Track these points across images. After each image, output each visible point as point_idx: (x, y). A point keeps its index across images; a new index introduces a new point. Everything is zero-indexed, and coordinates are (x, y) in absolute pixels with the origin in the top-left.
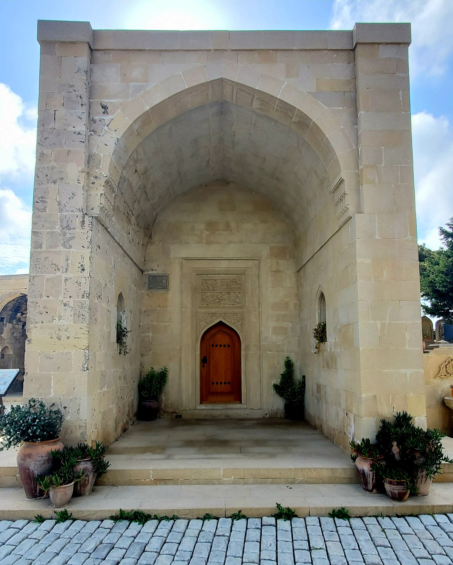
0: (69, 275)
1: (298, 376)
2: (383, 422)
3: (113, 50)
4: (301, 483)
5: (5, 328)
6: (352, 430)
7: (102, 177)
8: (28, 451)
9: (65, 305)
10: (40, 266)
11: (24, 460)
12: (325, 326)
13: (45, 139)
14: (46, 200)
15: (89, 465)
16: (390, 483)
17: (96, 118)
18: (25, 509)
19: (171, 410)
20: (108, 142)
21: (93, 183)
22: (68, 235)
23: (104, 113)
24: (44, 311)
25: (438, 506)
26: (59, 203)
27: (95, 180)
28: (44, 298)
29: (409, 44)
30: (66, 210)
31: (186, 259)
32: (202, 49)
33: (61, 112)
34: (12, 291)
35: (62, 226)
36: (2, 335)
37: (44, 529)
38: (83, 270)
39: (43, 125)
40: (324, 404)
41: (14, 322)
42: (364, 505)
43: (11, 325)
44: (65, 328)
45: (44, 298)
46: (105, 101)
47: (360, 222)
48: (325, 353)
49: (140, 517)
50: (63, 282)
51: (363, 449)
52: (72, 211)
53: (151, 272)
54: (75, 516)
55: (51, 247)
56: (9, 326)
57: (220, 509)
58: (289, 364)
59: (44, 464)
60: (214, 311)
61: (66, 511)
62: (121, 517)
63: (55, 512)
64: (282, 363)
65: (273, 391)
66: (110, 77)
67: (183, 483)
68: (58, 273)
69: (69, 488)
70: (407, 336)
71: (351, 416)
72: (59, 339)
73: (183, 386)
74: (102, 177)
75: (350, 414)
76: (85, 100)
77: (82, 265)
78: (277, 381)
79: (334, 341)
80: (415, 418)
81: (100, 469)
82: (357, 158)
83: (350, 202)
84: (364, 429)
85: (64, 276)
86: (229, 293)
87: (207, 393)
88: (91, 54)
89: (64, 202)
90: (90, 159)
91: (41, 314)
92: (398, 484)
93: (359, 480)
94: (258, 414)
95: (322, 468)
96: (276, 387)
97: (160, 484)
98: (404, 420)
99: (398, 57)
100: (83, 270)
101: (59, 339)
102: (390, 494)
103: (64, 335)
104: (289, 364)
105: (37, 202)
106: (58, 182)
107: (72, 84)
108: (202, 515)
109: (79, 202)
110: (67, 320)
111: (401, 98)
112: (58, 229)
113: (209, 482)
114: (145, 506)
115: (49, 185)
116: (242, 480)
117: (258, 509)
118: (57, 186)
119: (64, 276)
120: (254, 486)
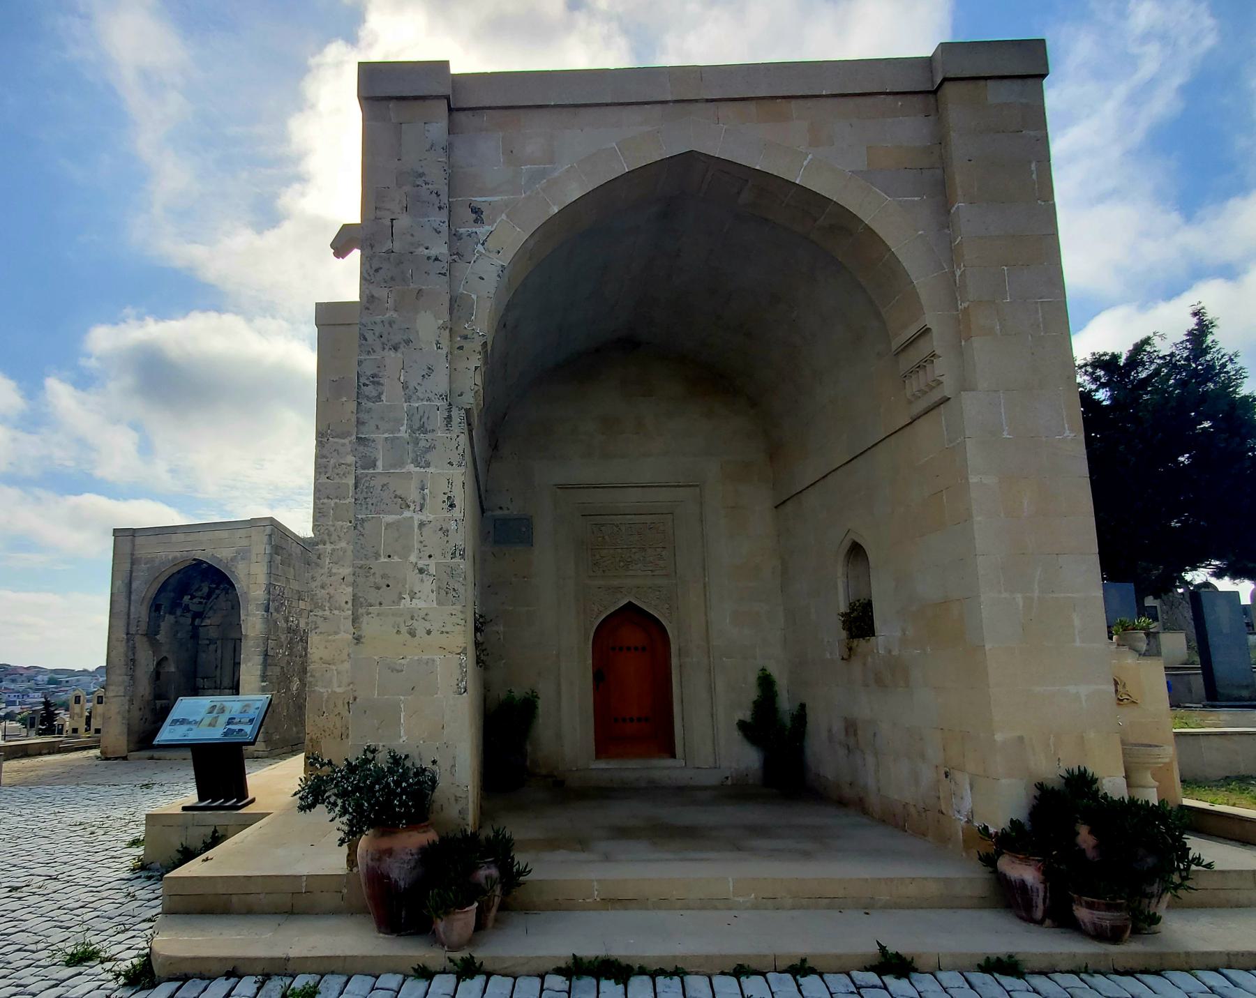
0: (425, 516)
1: (785, 704)
2: (1040, 786)
3: (489, 108)
4: (886, 907)
5: (162, 624)
6: (967, 804)
7: (476, 336)
8: (386, 843)
9: (421, 571)
10: (374, 501)
11: (379, 859)
12: (868, 606)
13: (377, 271)
14: (381, 381)
15: (494, 872)
16: (1090, 906)
17: (462, 230)
18: (375, 953)
19: (544, 772)
20: (487, 273)
21: (461, 348)
22: (422, 444)
23: (476, 221)
24: (383, 583)
25: (1196, 954)
26: (405, 387)
27: (463, 343)
28: (383, 560)
29: (1044, 76)
30: (418, 398)
31: (562, 487)
32: (494, 104)
33: (404, 221)
34: (178, 554)
35: (411, 427)
36: (158, 637)
37: (441, 991)
38: (452, 506)
39: (372, 246)
40: (870, 760)
41: (179, 612)
42: (1045, 950)
43: (172, 617)
44: (422, 614)
45: (383, 560)
46: (478, 200)
47: (972, 407)
48: (870, 659)
49: (618, 971)
50: (416, 530)
51: (1014, 840)
52: (429, 400)
53: (498, 513)
54: (488, 966)
55: (394, 466)
56: (170, 619)
57: (765, 956)
58: (766, 682)
59: (414, 868)
60: (616, 583)
61: (472, 957)
62: (575, 969)
63: (451, 960)
64: (753, 679)
65: (737, 735)
66: (487, 155)
67: (657, 907)
68: (407, 514)
69: (468, 916)
70: (1077, 622)
71: (963, 780)
72: (412, 634)
73: (566, 725)
74: (476, 336)
75: (958, 775)
76: (444, 199)
77: (449, 498)
78: (746, 714)
79: (898, 634)
80: (1104, 781)
81: (511, 878)
82: (954, 289)
83: (943, 368)
84: (1004, 805)
85: (418, 517)
86: (644, 550)
87: (609, 739)
88: (450, 115)
89: (412, 384)
90: (456, 305)
91: (378, 588)
92: (1109, 908)
93: (1010, 898)
94: (712, 779)
95: (926, 879)
96: (742, 725)
97: (614, 908)
98: (1081, 783)
99: (1024, 101)
100: (452, 506)
101: (412, 634)
102: (1090, 928)
103: (420, 627)
104: (766, 682)
105: (365, 385)
106: (402, 348)
107: (421, 171)
108: (730, 967)
109: (440, 382)
110: (425, 599)
111: (1034, 176)
112: (403, 432)
113: (707, 904)
114: (621, 949)
115: (386, 353)
116: (771, 902)
117: (839, 957)
118: (399, 355)
119: (418, 517)
120: (796, 913)
